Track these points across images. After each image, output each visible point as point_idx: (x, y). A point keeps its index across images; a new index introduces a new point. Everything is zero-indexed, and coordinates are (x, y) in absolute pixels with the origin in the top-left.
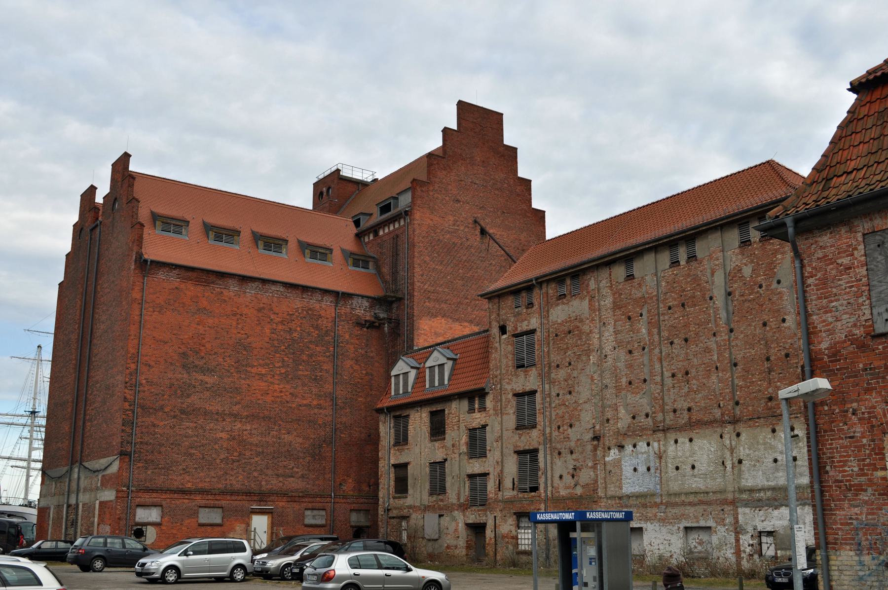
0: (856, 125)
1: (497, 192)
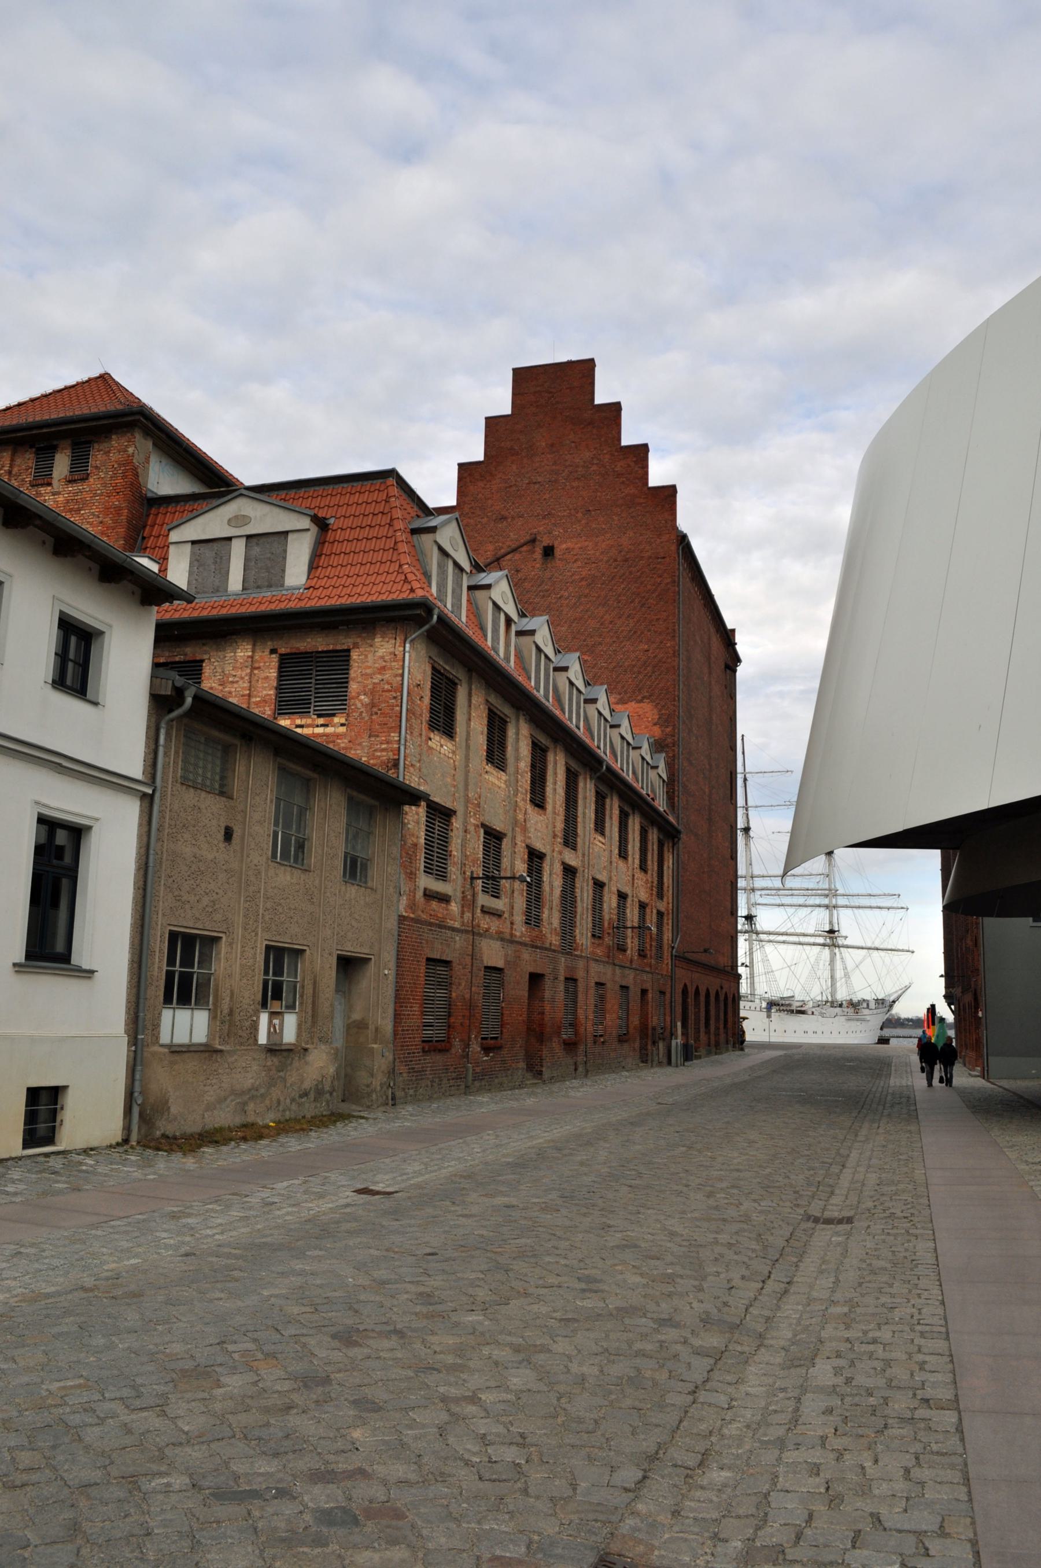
0: (819, 906)
1: (575, 484)
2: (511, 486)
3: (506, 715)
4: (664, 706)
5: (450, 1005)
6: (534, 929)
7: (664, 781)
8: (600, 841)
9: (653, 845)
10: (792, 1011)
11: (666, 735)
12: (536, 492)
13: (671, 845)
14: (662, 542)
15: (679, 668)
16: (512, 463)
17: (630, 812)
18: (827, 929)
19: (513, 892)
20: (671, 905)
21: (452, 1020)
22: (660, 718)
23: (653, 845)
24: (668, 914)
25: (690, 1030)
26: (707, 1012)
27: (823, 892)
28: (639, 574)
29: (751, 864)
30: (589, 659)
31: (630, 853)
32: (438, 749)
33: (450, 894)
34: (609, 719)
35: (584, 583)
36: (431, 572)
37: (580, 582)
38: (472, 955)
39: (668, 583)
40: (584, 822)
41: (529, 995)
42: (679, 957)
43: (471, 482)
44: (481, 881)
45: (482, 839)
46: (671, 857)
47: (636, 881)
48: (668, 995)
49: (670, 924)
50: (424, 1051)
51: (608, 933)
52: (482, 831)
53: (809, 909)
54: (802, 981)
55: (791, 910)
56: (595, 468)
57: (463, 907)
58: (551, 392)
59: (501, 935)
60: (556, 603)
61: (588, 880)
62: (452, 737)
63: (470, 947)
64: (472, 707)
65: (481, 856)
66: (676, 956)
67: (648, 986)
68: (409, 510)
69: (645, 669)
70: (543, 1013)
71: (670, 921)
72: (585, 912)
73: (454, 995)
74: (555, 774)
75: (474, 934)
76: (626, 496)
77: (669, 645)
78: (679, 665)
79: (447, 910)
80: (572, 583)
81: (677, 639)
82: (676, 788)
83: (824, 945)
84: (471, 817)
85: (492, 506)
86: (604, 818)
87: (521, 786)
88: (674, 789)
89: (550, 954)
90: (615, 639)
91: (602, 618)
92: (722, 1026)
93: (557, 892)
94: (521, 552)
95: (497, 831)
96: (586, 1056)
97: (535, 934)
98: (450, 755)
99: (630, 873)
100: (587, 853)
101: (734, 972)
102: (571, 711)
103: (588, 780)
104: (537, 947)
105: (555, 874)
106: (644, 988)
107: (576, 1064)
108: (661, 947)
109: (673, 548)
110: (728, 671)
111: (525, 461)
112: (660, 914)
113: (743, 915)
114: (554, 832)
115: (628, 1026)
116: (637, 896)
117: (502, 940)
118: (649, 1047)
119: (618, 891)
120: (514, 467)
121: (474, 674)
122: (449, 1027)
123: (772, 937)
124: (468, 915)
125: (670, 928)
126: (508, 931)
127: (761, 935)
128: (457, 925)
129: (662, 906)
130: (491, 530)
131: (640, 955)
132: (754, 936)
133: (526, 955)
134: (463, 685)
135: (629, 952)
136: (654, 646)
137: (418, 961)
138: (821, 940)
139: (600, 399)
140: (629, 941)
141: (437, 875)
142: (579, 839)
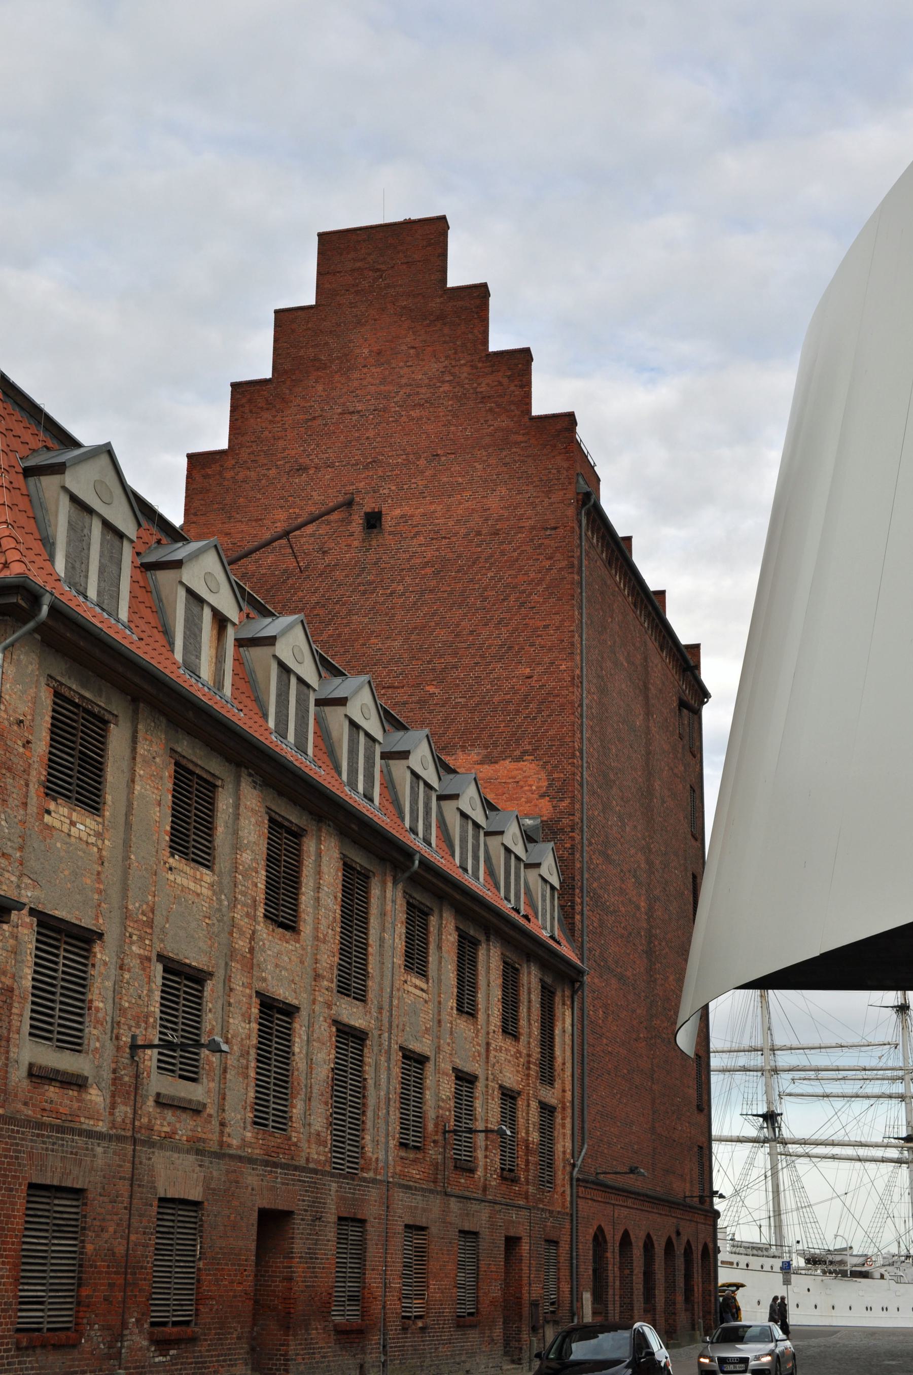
1: (415, 414)
2: (314, 418)
3: (213, 775)
4: (556, 766)
5: (81, 1266)
6: (272, 1134)
7: (553, 888)
8: (416, 987)
9: (529, 993)
10: (844, 1274)
11: (561, 812)
12: (354, 426)
13: (568, 993)
14: (551, 504)
15: (581, 705)
16: (316, 382)
17: (482, 938)
18: (904, 1135)
19: (225, 1071)
20: (568, 1094)
21: (85, 1292)
22: (550, 786)
23: (529, 993)
24: (564, 1109)
25: (610, 1307)
26: (648, 1275)
27: (895, 1073)
28: (515, 554)
29: (769, 1029)
30: (437, 691)
31: (481, 1006)
32: (65, 828)
33: (86, 1074)
34: (435, 784)
35: (429, 570)
36: (55, 538)
37: (424, 568)
38: (132, 1179)
39: (561, 569)
40: (381, 955)
41: (258, 1248)
42: (586, 1181)
43: (251, 411)
44: (156, 1051)
45: (159, 981)
46: (568, 1013)
47: (493, 1053)
48: (564, 1247)
49: (568, 1125)
50: (18, 1349)
51: (435, 1142)
52: (160, 967)
53: (867, 1102)
54: (865, 1223)
55: (838, 1103)
56: (446, 387)
57: (113, 1096)
58: (378, 270)
59: (201, 1145)
60: (383, 603)
61: (388, 1052)
62: (97, 809)
63: (129, 1165)
64: (138, 759)
65: (156, 1009)
66: (578, 1180)
67: (521, 1231)
68: (27, 436)
69: (526, 707)
70: (290, 1279)
71: (568, 1121)
72: (382, 1105)
73: (89, 1248)
74: (319, 873)
75: (135, 1141)
76: (496, 430)
77: (563, 667)
78: (581, 700)
79: (80, 1100)
80: (410, 570)
81: (578, 658)
82: (578, 900)
83: (899, 1161)
84: (132, 943)
85: (284, 449)
86: (427, 949)
87: (242, 893)
88: (573, 902)
89: (305, 1177)
90: (477, 659)
91: (458, 625)
92: (680, 1298)
93: (323, 1072)
94: (329, 523)
95: (194, 968)
96: (385, 1353)
97: (273, 1142)
98: (92, 840)
99: (481, 1039)
100: (386, 1006)
101: (706, 1207)
102: (353, 771)
103: (390, 885)
104: (276, 1165)
105: (318, 1040)
106: (512, 1233)
107: (362, 1366)
108: (550, 1165)
109: (571, 512)
110: (685, 711)
111: (337, 378)
112: (547, 1110)
113: (760, 1112)
114: (315, 970)
115: (477, 1301)
116: (495, 1079)
117: (198, 1152)
118: (525, 1336)
119: (454, 1069)
120: (320, 388)
121: (142, 705)
122: (79, 1304)
123: (808, 1149)
124: (123, 1110)
125: (568, 1132)
126: (215, 1137)
127: (789, 1146)
128: (102, 1127)
129: (551, 1096)
130: (283, 488)
131: (503, 1178)
132: (780, 1148)
133: (251, 1178)
134: (121, 722)
135: (480, 1173)
136: (540, 669)
137: (11, 1190)
138: (893, 1153)
139: (456, 278)
140: (480, 1154)
141: (59, 1040)
142: (370, 983)
